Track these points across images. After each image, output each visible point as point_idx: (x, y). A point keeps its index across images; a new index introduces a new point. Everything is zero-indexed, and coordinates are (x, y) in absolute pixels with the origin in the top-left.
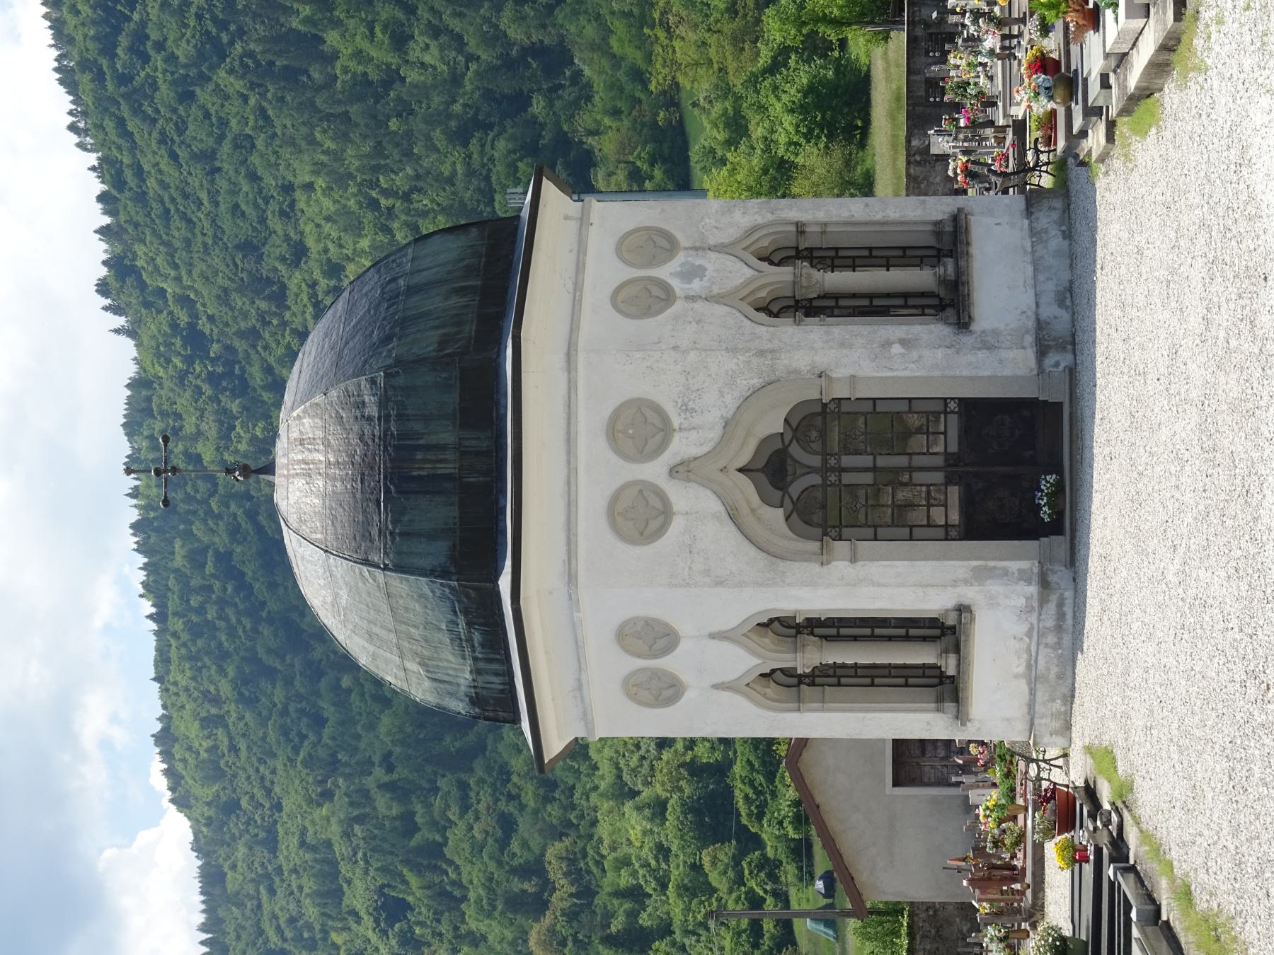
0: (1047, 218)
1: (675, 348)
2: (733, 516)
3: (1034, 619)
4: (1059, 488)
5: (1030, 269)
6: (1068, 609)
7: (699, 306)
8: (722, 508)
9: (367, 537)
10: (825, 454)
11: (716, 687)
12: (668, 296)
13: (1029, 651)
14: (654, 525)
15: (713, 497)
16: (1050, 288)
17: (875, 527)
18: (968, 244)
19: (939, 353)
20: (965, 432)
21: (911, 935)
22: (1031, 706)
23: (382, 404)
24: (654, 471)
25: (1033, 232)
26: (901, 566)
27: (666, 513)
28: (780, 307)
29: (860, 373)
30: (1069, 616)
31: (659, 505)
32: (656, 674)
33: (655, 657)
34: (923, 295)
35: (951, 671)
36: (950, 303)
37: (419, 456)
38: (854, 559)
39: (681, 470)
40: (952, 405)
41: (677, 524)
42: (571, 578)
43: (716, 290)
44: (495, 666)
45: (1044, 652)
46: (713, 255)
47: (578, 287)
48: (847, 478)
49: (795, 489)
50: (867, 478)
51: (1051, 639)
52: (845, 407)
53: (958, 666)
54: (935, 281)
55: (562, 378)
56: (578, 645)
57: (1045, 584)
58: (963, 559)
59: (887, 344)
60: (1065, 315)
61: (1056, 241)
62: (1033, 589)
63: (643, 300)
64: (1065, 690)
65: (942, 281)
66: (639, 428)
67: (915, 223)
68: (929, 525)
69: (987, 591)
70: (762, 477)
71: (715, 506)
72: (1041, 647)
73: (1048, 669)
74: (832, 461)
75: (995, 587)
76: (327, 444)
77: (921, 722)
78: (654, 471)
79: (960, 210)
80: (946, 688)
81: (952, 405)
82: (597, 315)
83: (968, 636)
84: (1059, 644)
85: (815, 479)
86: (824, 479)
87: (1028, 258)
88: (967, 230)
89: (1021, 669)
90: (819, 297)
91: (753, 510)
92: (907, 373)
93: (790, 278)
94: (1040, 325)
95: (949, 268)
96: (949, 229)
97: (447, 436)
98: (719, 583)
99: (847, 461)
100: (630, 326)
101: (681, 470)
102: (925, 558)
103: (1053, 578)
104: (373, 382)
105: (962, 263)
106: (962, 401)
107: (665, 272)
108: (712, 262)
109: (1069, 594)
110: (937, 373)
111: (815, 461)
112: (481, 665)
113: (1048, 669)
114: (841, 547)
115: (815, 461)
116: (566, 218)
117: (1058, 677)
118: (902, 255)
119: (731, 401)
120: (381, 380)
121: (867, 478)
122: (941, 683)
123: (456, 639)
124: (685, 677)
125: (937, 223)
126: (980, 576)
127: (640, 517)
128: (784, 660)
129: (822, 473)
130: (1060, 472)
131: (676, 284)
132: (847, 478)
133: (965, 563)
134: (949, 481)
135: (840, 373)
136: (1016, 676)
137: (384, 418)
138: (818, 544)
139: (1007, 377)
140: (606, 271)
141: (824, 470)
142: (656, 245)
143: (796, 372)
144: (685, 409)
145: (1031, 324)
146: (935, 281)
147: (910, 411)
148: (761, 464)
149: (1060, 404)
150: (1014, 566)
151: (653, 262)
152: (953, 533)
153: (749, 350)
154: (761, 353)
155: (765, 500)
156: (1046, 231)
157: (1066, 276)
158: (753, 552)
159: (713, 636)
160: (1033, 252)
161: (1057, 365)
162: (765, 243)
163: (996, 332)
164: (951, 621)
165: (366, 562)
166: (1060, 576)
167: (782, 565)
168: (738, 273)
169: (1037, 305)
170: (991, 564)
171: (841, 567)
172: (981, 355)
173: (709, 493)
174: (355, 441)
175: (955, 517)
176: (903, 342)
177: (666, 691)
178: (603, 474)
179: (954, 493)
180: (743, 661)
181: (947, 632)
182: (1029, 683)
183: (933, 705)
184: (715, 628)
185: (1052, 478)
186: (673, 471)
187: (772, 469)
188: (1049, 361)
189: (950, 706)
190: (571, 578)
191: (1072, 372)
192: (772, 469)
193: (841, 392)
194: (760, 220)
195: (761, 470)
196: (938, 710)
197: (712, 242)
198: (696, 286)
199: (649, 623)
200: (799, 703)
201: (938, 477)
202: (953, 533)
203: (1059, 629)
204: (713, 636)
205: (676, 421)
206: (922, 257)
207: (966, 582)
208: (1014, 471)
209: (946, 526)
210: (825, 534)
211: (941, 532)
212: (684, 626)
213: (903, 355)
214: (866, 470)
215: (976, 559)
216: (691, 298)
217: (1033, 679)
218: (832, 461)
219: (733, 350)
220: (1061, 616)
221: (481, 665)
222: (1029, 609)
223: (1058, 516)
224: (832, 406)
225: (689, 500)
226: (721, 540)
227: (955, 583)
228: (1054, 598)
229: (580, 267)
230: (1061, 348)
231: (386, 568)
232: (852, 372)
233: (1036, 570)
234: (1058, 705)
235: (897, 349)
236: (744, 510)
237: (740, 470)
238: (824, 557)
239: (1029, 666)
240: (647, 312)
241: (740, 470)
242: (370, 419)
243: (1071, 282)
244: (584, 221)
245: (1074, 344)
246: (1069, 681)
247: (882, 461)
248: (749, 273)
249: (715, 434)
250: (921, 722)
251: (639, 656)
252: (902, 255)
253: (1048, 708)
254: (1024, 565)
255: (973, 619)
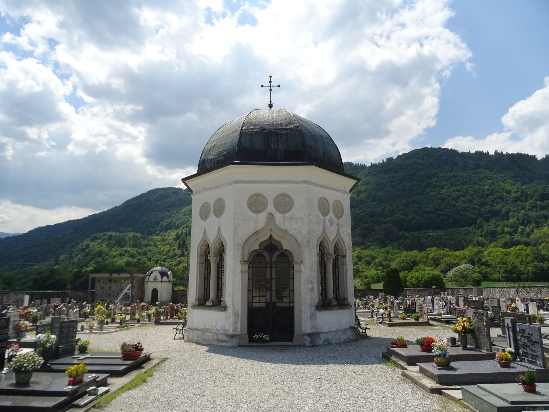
0: (349, 334)
1: (310, 215)
2: (256, 233)
3: (222, 332)
4: (264, 341)
5: (334, 329)
6: (224, 344)
7: (322, 224)
8: (259, 229)
9: (251, 125)
10: (276, 263)
11: (205, 230)
12: (325, 214)
13: (212, 329)
14: (254, 208)
15: (262, 227)
16: (329, 337)
17: (252, 279)
18: (342, 309)
19: (309, 300)
20: (283, 308)
21: (183, 290)
22: (196, 329)
23: (290, 129)
24: (271, 208)
25: (346, 329)
26: (239, 287)
27: (257, 212)
28: (322, 247)
29: (302, 274)
30: (222, 344)
31: (260, 210)
32: (209, 212)
33: (214, 211)
34: (326, 294)
35: (207, 304)
36: (324, 304)
37: (275, 139)
38: (242, 272)
39: (271, 217)
40: (292, 304)
41: (254, 215)
42: (237, 182)
43: (327, 229)
44: (213, 165)
45: (212, 334)
46: (336, 229)
47: (327, 188)
48: (268, 270)
49: (265, 253)
50: (268, 276)
51: (215, 338)
52: (291, 269)
53: (208, 306)
54: (331, 298)
55: (300, 180)
56: (217, 187)
57: (232, 336)
58: (241, 308)
59: (312, 283)
60: (321, 342)
61: (343, 337)
62: (231, 332)
63: (324, 207)
64: (200, 341)
65: (330, 301)
66: (284, 203)
67: (347, 292)
68: (253, 296)
69: (228, 319)
70: (269, 243)
71: (259, 227)
72: (213, 334)
73: (206, 336)
74: (274, 265)
75: (232, 319)
76: (278, 116)
77: (193, 292)
78: (271, 208)
79: (351, 306)
80: (202, 303)
81: (292, 304)
82: (318, 193)
83: (217, 309)
84: (214, 340)
85: (268, 259)
86: (268, 263)
87: (338, 329)
88: (345, 309)
89: (207, 327)
90: (324, 262)
91: (258, 239)
92: (302, 289)
93: (330, 252)
94: (318, 334)
95: (335, 303)
96: (346, 303)
97: (281, 147)
98: (235, 228)
99: (274, 270)
100: (316, 202)
101: (271, 217)
102: (242, 296)
103: (234, 339)
104: (297, 127)
105: (336, 307)
106: (293, 308)
107: (331, 215)
108: (334, 228)
109: (229, 345)
110: (302, 299)
111: (274, 259)
112: (213, 161)
113: (206, 336)
114: (246, 268)
115: (274, 259)
116: (345, 187)
117: (204, 339)
118: (337, 288)
119: (293, 232)
120: (298, 129)
121: (268, 276)
122: (205, 300)
123: (221, 152)
124: (208, 220)
125: (347, 299)
126: (236, 314)
127: (256, 204)
128: (212, 250)
129: (270, 262)
130: (271, 340)
131: (328, 217)
132: (268, 270)
133: (240, 309)
134: (267, 303)
135: (302, 268)
136: (205, 325)
137: (287, 129)
138: (247, 260)
139: (301, 323)
140: (332, 197)
141: (271, 262)
142: (339, 214)
143: (303, 253)
144: (290, 218)
145: (319, 331)
146: (331, 298)
147: (290, 290)
148: (273, 242)
149: (292, 341)
150: (239, 326)
151: (334, 211)
152: (250, 305)
153: (309, 238)
154: (308, 242)
155: (261, 244)
156: (346, 334)
157: (333, 342)
158: (245, 239)
159: (219, 228)
160: (340, 330)
161: (306, 340)
162: (340, 246)
163: (316, 319)
164: (222, 304)
165: (243, 125)
166: (235, 342)
167: (240, 249)
168: (331, 237)
169: (325, 333)
170: (240, 318)
171: (239, 267)
172: (309, 315)
173: (264, 225)
174: (280, 122)
175: (254, 305)
176: (312, 288)
177: (204, 216)
178: (270, 192)
179: (264, 305)
180: (212, 238)
181: (219, 304)
182: (203, 329)
183: (198, 297)
184: (221, 228)
185: (268, 339)
186: (271, 214)
187: (271, 246)
188: (307, 338)
189: (197, 303)
190: (237, 182)
191: (304, 346)
192: (271, 246)
193: (296, 268)
194: (346, 244)
195: (271, 242)
196: (196, 299)
197: (340, 229)
198: (328, 223)
199: (223, 208)
200: (200, 256)
201: (269, 300)
202: (250, 305)
203: (218, 340)
204: (219, 228)
205: (287, 215)
206: (336, 294)
207: (234, 309)
208: (270, 329)
209: (253, 302)
210: (250, 263)
211: (250, 301)
212: (222, 218)
213: (308, 288)
214: (271, 276)
215: (241, 313)
216: (324, 221)
217: (204, 330)
218: (274, 265)
219: (309, 233)
220: (222, 341)
221: (213, 161)
222: (225, 330)
223: (255, 341)
224: (291, 265)
225: (261, 220)
226: (248, 229)
227: (233, 305)
228: (228, 339)
229: (332, 189)
230: (311, 342)
231: (241, 130)
232: (303, 271)
233: (237, 333)
234: (196, 338)
235: (310, 286)
236: (258, 236)
237: (271, 236)
238: (243, 262)
239: (208, 329)
240: (320, 208)
241: (271, 236)
242: (286, 126)
243: (331, 344)
244: (344, 192)
245: (313, 346)
246: (203, 343)
247: (274, 282)
248: (332, 240)
249: (282, 227)
250: (193, 292)
251: (214, 206)
252: (337, 288)
253: (195, 335)
254: (239, 329)
255: (222, 311)
